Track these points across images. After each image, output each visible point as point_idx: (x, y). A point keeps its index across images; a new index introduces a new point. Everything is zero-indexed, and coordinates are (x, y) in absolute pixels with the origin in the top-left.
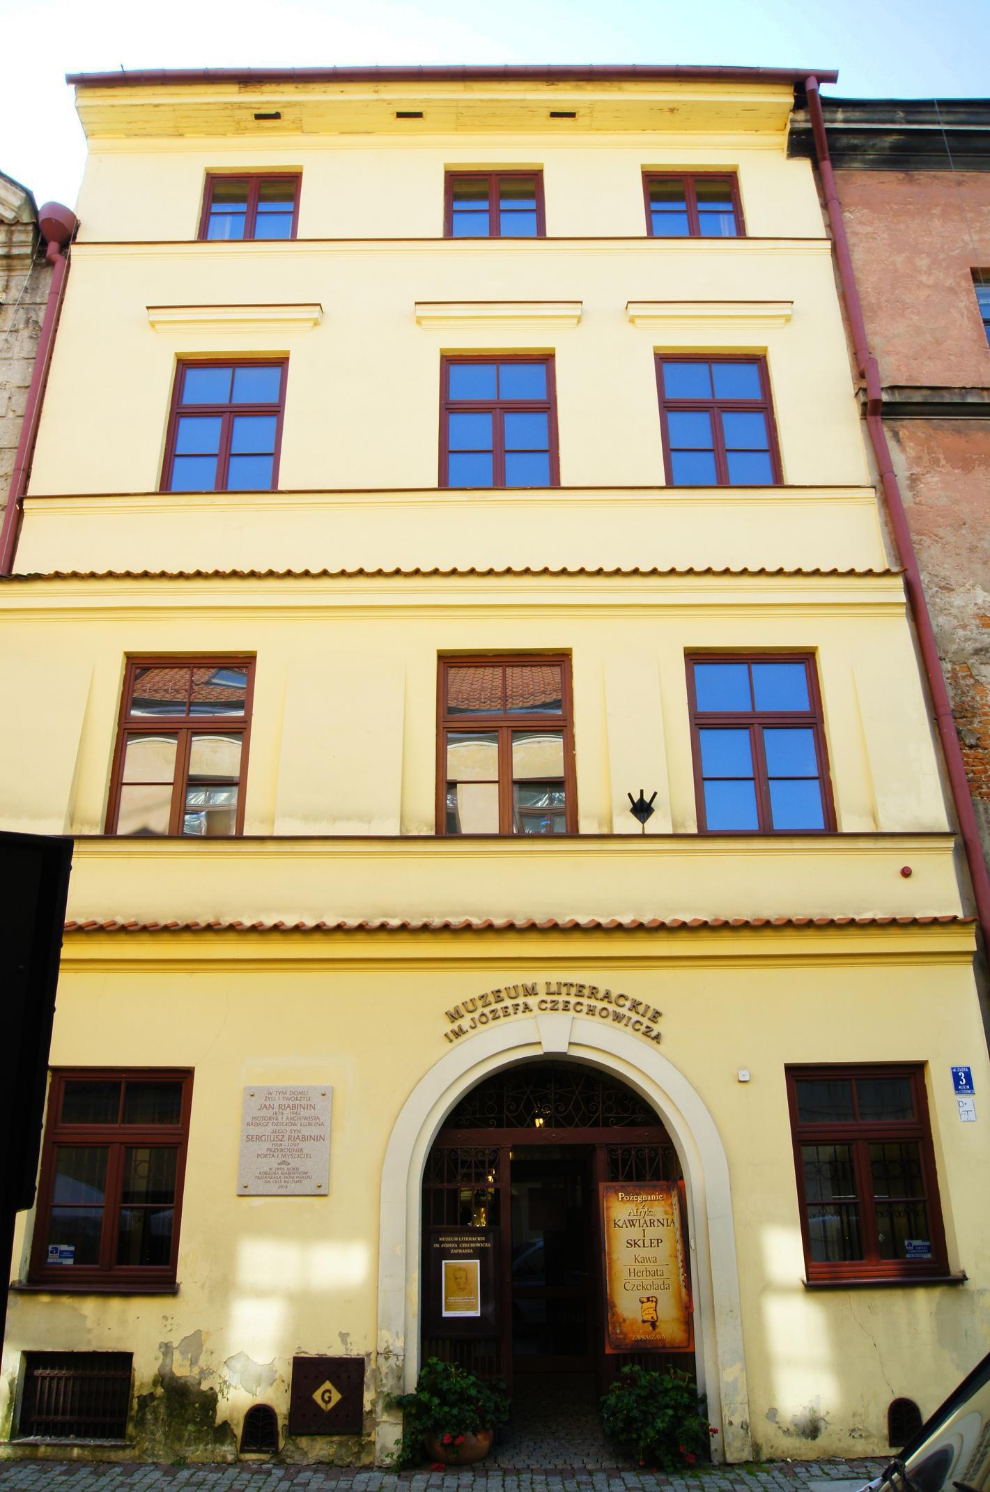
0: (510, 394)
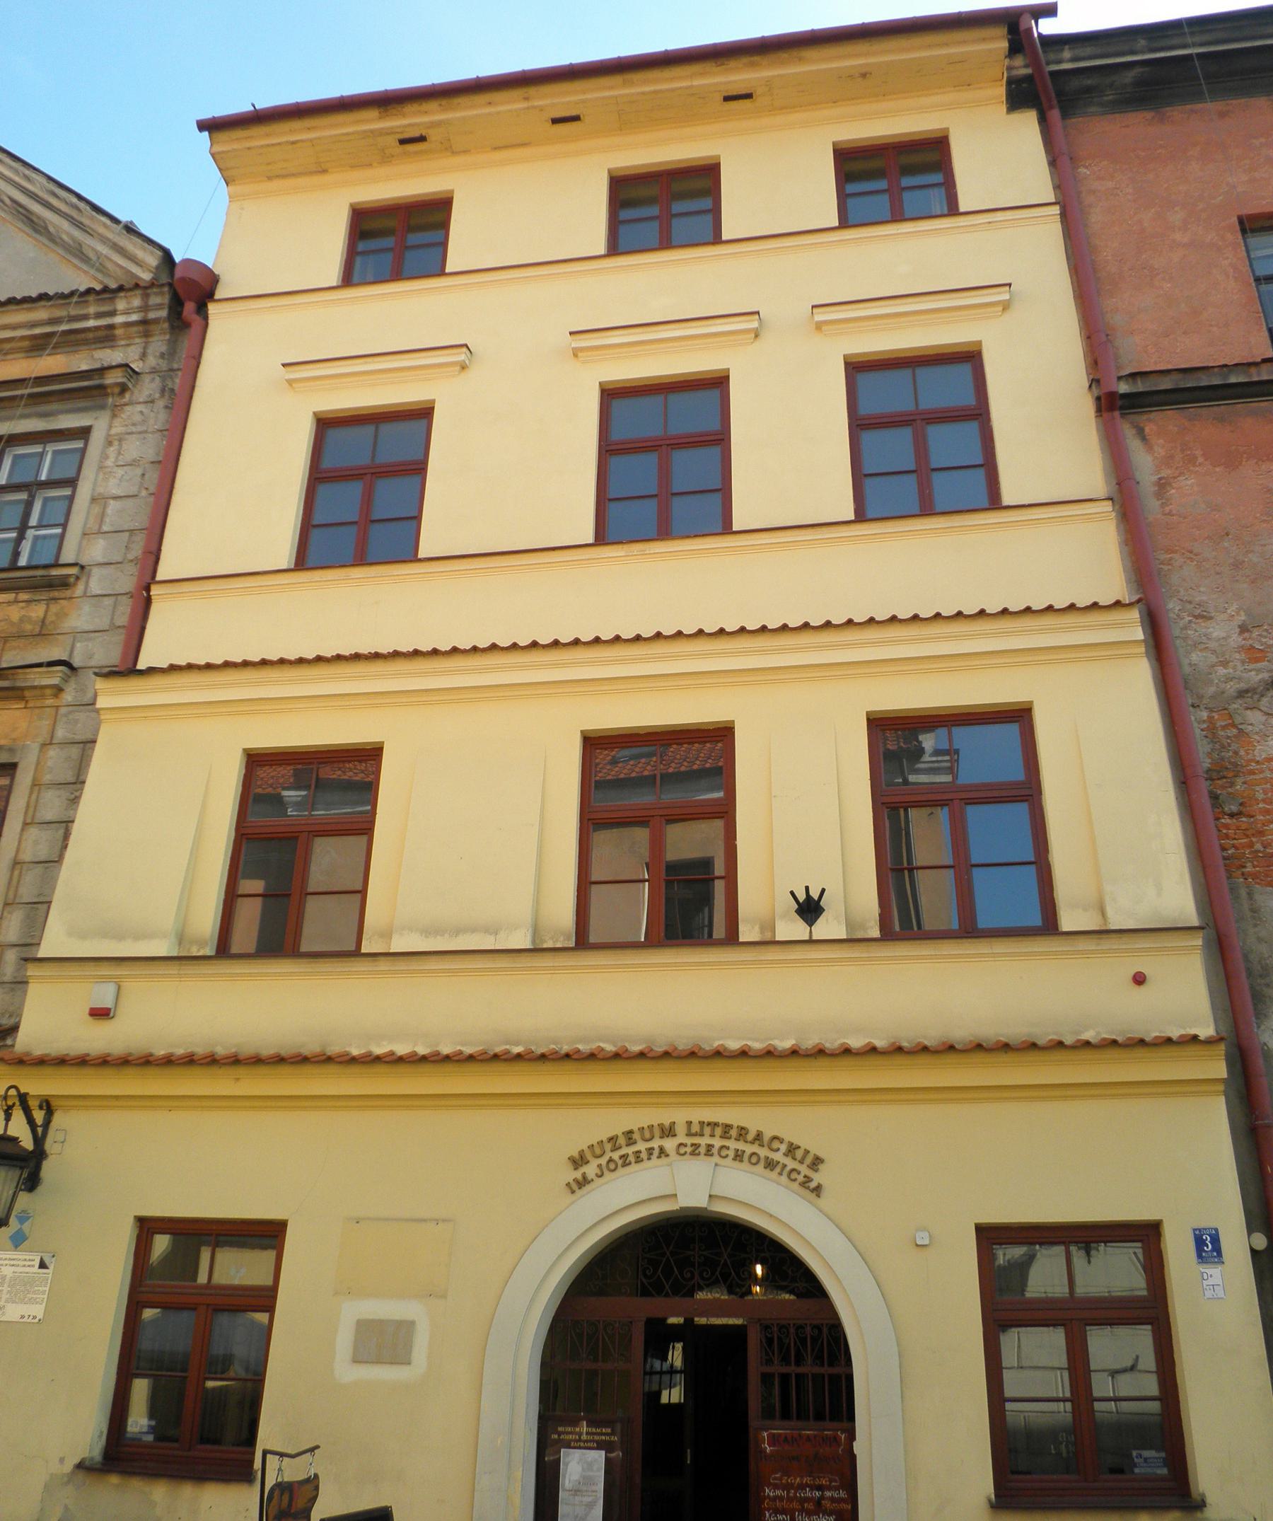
0: (930, 401)
